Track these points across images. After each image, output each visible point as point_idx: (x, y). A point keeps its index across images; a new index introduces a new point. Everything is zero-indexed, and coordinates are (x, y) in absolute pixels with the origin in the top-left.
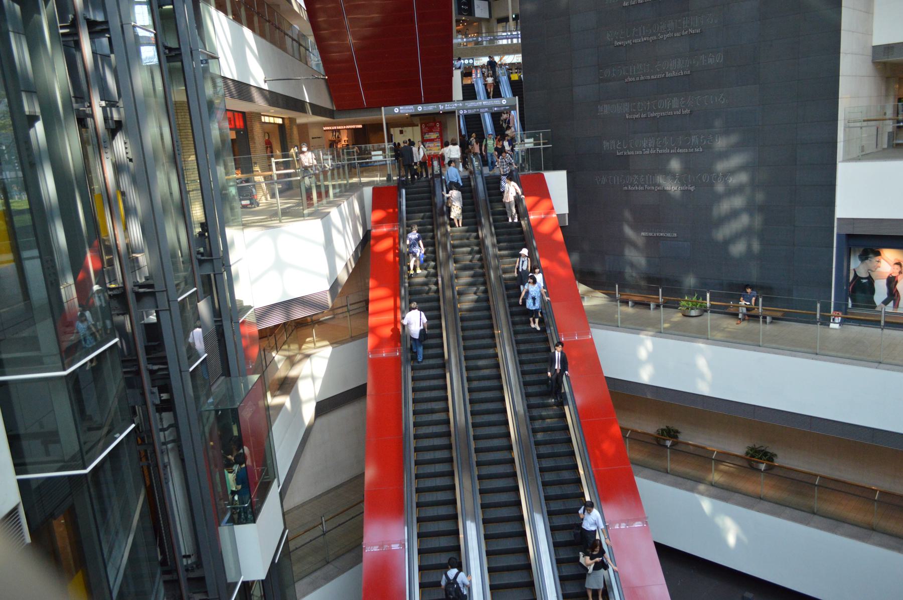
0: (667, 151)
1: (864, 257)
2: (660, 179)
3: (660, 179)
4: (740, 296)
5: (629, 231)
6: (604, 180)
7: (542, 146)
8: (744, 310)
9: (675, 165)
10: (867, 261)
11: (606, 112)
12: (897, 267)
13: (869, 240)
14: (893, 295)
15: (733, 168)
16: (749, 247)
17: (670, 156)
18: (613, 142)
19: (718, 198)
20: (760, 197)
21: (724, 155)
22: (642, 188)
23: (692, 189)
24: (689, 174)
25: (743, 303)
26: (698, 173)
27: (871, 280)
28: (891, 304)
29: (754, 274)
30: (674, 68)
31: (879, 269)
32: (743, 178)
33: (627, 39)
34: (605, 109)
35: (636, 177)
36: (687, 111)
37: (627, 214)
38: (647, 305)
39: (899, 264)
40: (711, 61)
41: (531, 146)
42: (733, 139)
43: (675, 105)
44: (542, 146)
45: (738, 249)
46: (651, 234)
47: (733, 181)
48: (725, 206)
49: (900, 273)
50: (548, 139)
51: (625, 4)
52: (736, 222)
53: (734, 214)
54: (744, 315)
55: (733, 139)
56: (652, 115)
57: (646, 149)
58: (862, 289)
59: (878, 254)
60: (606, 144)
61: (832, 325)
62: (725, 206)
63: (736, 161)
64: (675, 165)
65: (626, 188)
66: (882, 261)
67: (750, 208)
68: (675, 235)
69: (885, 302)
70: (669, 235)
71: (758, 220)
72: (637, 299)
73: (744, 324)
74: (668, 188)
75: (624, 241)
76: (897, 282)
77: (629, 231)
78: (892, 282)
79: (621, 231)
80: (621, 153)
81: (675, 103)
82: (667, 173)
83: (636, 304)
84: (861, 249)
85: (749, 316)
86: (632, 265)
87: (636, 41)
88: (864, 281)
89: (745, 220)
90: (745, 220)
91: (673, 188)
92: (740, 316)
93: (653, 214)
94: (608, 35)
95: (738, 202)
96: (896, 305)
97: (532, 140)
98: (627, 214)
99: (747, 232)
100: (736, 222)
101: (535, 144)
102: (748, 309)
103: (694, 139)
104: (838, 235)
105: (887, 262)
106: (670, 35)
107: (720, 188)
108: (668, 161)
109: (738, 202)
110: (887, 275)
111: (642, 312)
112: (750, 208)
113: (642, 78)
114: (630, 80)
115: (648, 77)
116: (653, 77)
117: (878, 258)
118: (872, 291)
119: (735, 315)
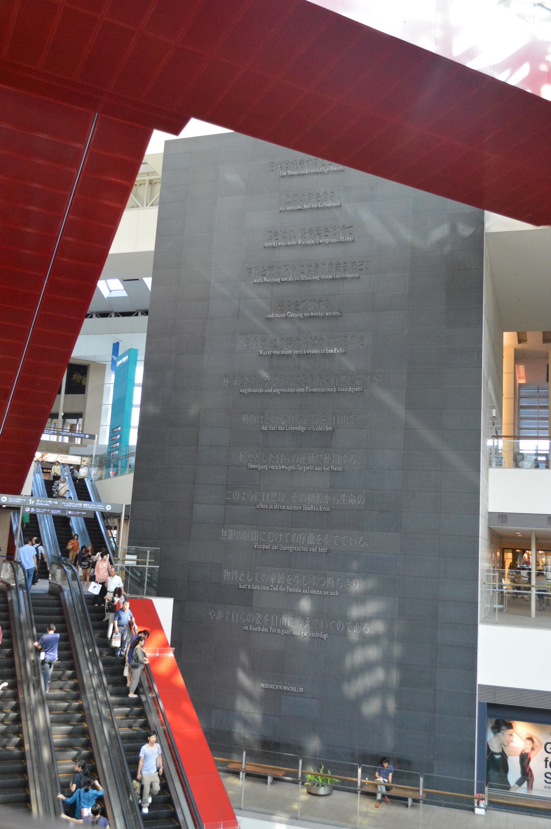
0: (296, 590)
1: (497, 729)
2: (287, 621)
3: (287, 621)
4: (375, 770)
5: (243, 678)
6: (220, 616)
7: (147, 566)
8: (384, 788)
9: (305, 605)
10: (500, 734)
11: (230, 537)
12: (529, 742)
13: (505, 711)
14: (526, 775)
15: (369, 615)
16: (384, 708)
17: (301, 595)
18: (236, 572)
19: (352, 647)
20: (397, 650)
21: (361, 599)
22: (266, 630)
23: (325, 636)
24: (315, 619)
25: (381, 779)
26: (330, 619)
27: (504, 756)
28: (525, 784)
29: (388, 742)
30: (313, 502)
31: (511, 744)
32: (377, 627)
33: (264, 464)
34: (230, 534)
35: (259, 616)
36: (323, 550)
37: (243, 658)
38: (263, 778)
39: (531, 739)
40: (352, 501)
41: (134, 563)
42: (371, 583)
43: (310, 539)
44: (147, 566)
45: (372, 708)
46: (272, 687)
47: (369, 629)
48: (359, 656)
49: (533, 749)
50: (157, 558)
51: (265, 428)
52: (370, 678)
53: (368, 667)
54: (383, 796)
55: (371, 583)
56: (284, 548)
57: (274, 584)
58: (497, 765)
59: (510, 726)
60: (226, 574)
61: (478, 811)
62: (359, 656)
63: (372, 607)
64: (305, 605)
65: (246, 628)
66: (514, 734)
67: (386, 662)
68: (301, 690)
69: (520, 783)
70: (294, 689)
71: (395, 676)
72: (251, 769)
73: (384, 809)
74: (297, 633)
75: (237, 689)
76: (529, 760)
77: (243, 678)
78: (525, 759)
79: (234, 677)
80: (244, 586)
81: (311, 539)
82: (297, 614)
83: (249, 775)
84: (494, 720)
85: (390, 797)
86: (246, 723)
87: (272, 467)
88: (498, 757)
89: (379, 675)
90: (379, 675)
91: (301, 630)
92: (379, 797)
93: (275, 663)
94: (241, 456)
95: (372, 653)
96: (530, 787)
97: (135, 557)
98: (243, 658)
99: (382, 690)
100: (370, 678)
101: (138, 563)
102: (388, 789)
103: (329, 581)
104: (479, 703)
105: (520, 736)
106: (311, 468)
107: (354, 634)
108: (298, 600)
109: (372, 653)
110: (519, 752)
111: (258, 786)
112: (386, 662)
113: (276, 507)
114: (262, 506)
115: (284, 507)
116: (288, 508)
117: (510, 731)
118: (506, 769)
119: (371, 795)
